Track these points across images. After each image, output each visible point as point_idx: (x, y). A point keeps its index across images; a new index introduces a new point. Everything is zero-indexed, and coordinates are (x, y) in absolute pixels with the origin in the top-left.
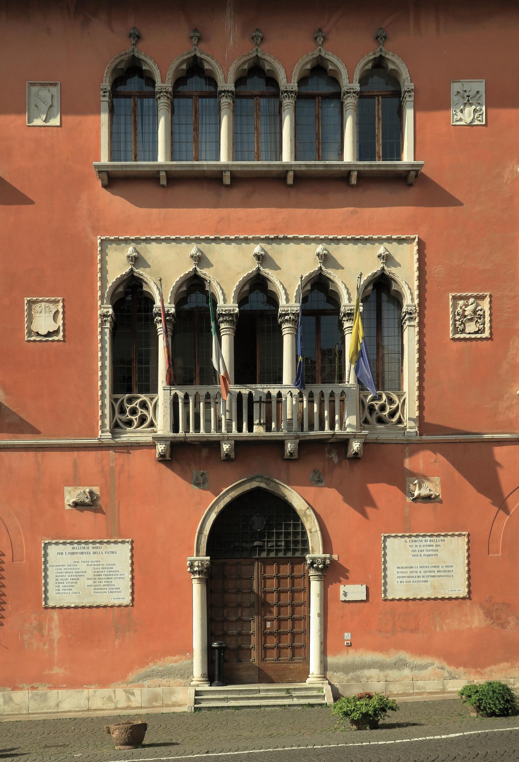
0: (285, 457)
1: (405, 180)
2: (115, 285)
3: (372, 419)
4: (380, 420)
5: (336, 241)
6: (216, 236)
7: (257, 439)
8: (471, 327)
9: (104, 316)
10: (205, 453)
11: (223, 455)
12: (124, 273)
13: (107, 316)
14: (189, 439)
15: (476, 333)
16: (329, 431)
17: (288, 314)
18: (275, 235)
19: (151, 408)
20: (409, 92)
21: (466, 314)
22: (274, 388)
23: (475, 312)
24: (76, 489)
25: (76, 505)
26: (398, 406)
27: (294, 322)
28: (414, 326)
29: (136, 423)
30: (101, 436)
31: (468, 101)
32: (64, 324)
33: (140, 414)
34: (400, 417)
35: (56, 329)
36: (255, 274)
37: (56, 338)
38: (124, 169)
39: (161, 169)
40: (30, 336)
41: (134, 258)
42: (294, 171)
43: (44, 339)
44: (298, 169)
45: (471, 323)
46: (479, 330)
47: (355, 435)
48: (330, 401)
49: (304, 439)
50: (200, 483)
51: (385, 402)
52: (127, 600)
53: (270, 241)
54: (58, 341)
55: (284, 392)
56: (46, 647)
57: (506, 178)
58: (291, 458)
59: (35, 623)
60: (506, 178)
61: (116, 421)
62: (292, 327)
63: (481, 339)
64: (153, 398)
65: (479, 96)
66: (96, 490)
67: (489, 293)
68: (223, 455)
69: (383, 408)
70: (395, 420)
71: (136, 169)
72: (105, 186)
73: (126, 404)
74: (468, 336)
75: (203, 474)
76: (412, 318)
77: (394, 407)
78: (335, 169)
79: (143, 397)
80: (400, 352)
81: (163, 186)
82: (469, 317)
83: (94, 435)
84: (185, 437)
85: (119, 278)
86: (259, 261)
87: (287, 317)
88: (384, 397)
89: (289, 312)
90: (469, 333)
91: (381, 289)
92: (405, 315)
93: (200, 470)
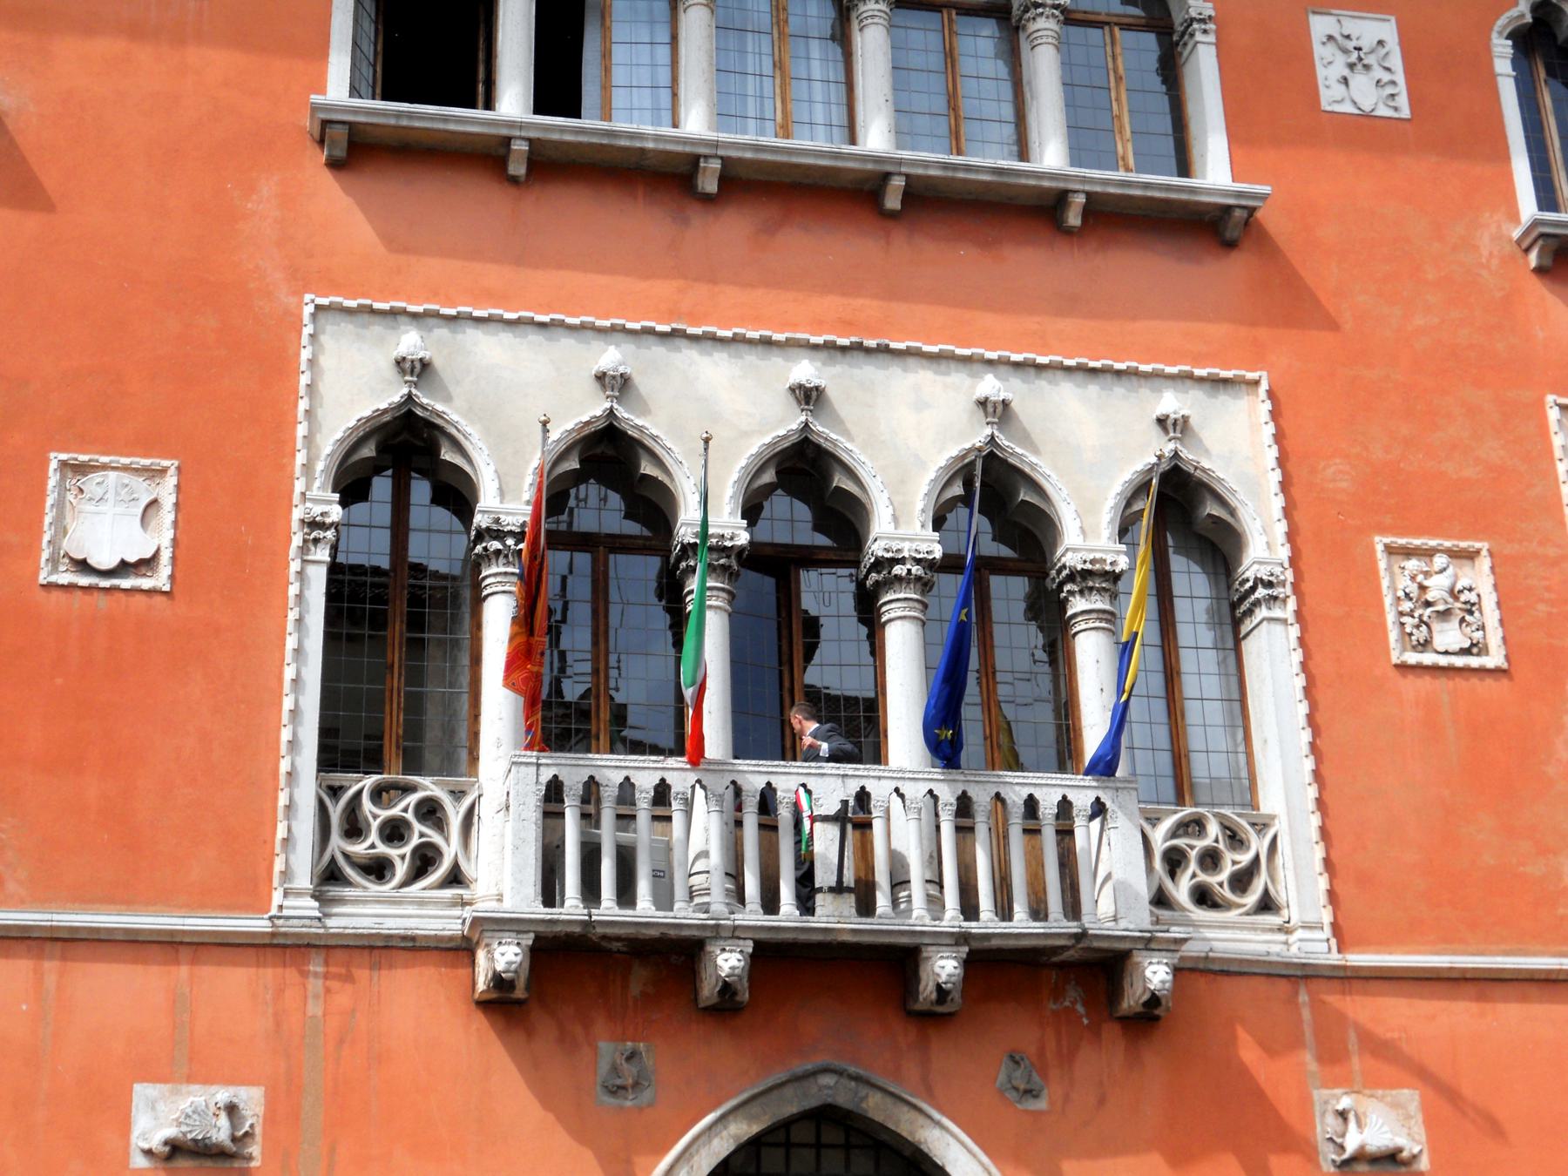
0: (918, 1007)
1: (1212, 227)
2: (354, 439)
4: (1203, 897)
5: (1032, 371)
6: (675, 326)
7: (829, 938)
8: (1449, 636)
9: (314, 525)
10: (639, 979)
11: (708, 991)
12: (383, 406)
13: (323, 526)
14: (600, 930)
15: (1465, 652)
16: (1065, 923)
17: (902, 561)
18: (854, 339)
20: (1202, 21)
21: (1430, 596)
22: (879, 778)
23: (1454, 594)
24: (177, 1093)
25: (176, 1149)
26: (1257, 858)
27: (919, 586)
28: (1284, 621)
29: (401, 870)
30: (281, 907)
31: (1360, 59)
32: (175, 541)
33: (415, 841)
34: (1266, 891)
35: (148, 555)
36: (794, 439)
37: (145, 583)
38: (404, 122)
39: (517, 133)
40: (55, 570)
41: (418, 366)
42: (908, 176)
43: (105, 583)
44: (920, 171)
45: (1446, 626)
46: (1473, 645)
47: (1150, 940)
48: (761, 826)
49: (986, 944)
50: (624, 1088)
51: (1217, 841)
53: (839, 354)
54: (151, 592)
55: (879, 791)
57: (1485, 253)
58: (940, 1009)
60: (1485, 253)
61: (333, 860)
62: (722, 590)
63: (1482, 671)
64: (463, 793)
65: (1382, 51)
66: (251, 1099)
67: (176, 463)
68: (708, 991)
69: (1211, 859)
70: (1252, 899)
71: (441, 126)
72: (334, 165)
73: (367, 804)
74: (1443, 661)
75: (632, 1056)
76: (1275, 598)
77: (1245, 858)
78: (1023, 181)
79: (429, 786)
80: (1236, 696)
81: (514, 180)
82: (1441, 607)
84: (588, 924)
85: (369, 419)
86: (807, 403)
87: (899, 570)
88: (1213, 829)
89: (906, 554)
90: (1446, 653)
91: (1178, 507)
92: (1253, 589)
93: (624, 1040)
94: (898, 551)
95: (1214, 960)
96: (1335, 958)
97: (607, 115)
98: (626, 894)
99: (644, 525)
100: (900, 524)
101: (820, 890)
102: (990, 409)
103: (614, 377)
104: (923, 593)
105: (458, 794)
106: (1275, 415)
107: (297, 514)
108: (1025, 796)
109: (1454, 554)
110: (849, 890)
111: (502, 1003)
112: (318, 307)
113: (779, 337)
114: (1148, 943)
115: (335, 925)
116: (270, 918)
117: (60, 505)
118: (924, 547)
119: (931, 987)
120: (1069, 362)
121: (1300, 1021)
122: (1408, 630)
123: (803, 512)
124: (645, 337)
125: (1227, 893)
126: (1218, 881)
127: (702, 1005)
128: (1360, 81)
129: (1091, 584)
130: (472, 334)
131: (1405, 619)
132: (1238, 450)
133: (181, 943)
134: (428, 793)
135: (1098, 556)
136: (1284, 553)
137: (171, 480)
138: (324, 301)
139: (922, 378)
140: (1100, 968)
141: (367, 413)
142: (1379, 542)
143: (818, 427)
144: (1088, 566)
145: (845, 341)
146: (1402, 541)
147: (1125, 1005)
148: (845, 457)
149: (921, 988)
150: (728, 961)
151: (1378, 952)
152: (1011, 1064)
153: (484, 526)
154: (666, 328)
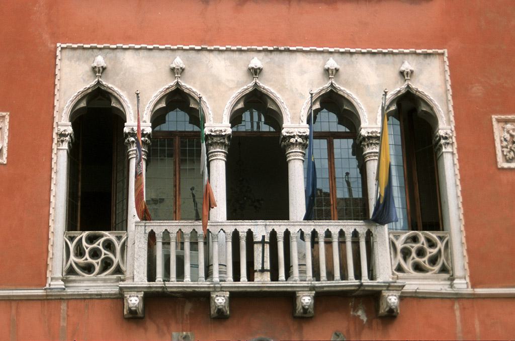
3: (408, 266)
4: (418, 268)
5: (349, 55)
10: (188, 307)
12: (88, 86)
13: (65, 135)
17: (294, 137)
18: (275, 47)
19: (118, 248)
26: (440, 251)
29: (97, 268)
41: (101, 69)
47: (389, 286)
53: (269, 54)
58: (305, 315)
61: (71, 265)
67: (8, 113)
68: (213, 311)
73: (84, 243)
79: (108, 235)
87: (292, 140)
88: (422, 239)
91: (410, 112)
94: (292, 132)
95: (419, 293)
96: (470, 290)
98: (180, 275)
99: (346, 127)
100: (138, 120)
101: (256, 271)
102: (330, 72)
103: (178, 69)
104: (303, 149)
107: (55, 131)
108: (326, 230)
110: (267, 271)
112: (62, 48)
113: (245, 48)
114: (389, 287)
115: (69, 291)
116: (45, 289)
118: (302, 130)
119: (300, 307)
120: (364, 51)
121: (455, 315)
122: (505, 154)
123: (333, 117)
124: (191, 52)
125: (427, 266)
126: (424, 261)
127: (212, 317)
129: (371, 142)
130: (120, 54)
131: (504, 149)
133: (13, 300)
134: (107, 237)
135: (374, 130)
138: (64, 46)
139: (300, 59)
140: (371, 298)
141: (82, 90)
142: (494, 117)
143: (182, 83)
144: (370, 135)
145: (271, 48)
146: (503, 117)
147: (380, 312)
148: (271, 96)
149: (297, 308)
151: (488, 287)
152: (336, 336)
153: (127, 132)
154: (199, 48)
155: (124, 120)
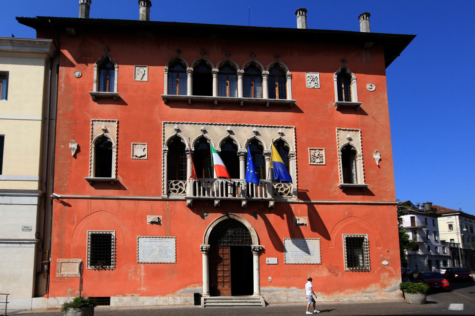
8: (318, 160)
9: (165, 150)
23: (319, 155)
29: (178, 192)
52: (174, 261)
56: (138, 279)
59: (133, 269)
66: (161, 217)
73: (173, 184)
77: (287, 189)
79: (181, 182)
83: (160, 196)
88: (283, 185)
91: (281, 145)
96: (297, 201)
97: (255, 97)
100: (242, 148)
105: (184, 183)
106: (295, 132)
109: (319, 150)
111: (189, 206)
117: (133, 149)
128: (313, 83)
132: (290, 138)
136: (295, 150)
137: (146, 146)
150: (216, 202)
155: (112, 144)
